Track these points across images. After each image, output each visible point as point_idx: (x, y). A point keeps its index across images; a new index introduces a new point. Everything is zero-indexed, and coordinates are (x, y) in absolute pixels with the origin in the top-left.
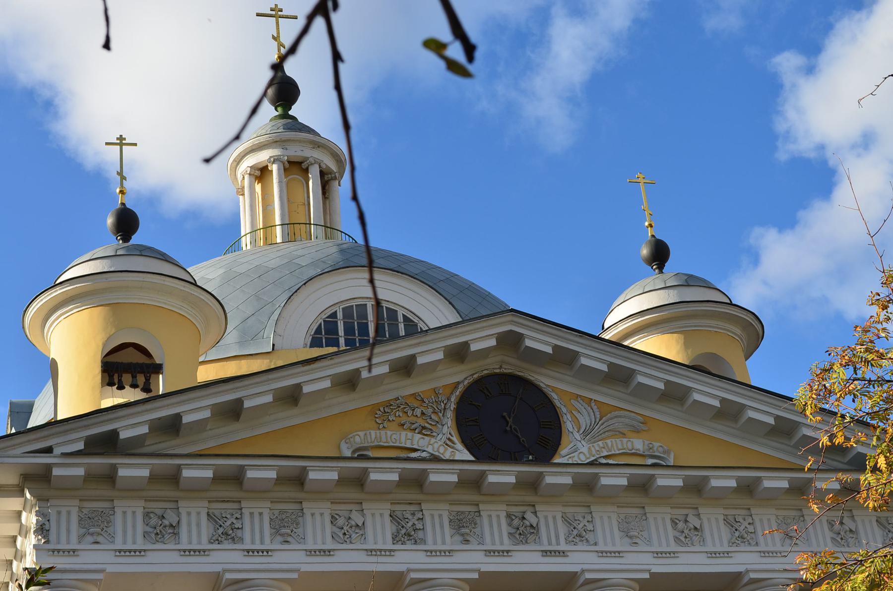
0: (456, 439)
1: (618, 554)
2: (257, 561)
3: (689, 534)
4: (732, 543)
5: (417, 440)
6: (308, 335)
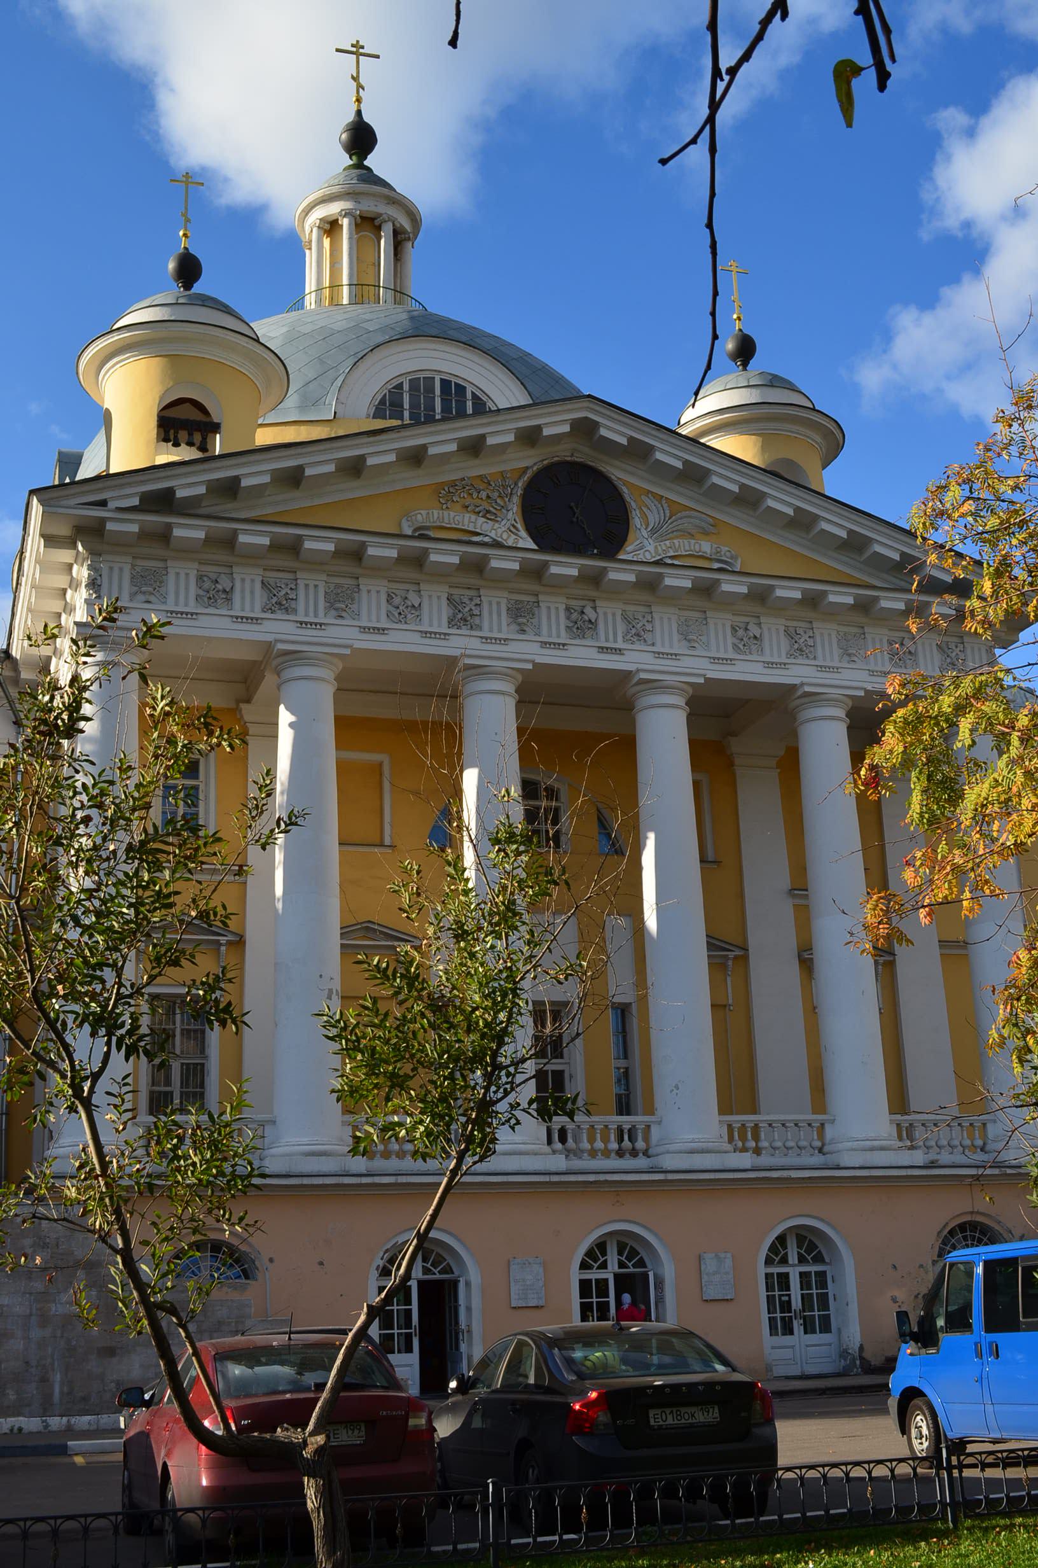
2: (310, 634)
5: (480, 524)
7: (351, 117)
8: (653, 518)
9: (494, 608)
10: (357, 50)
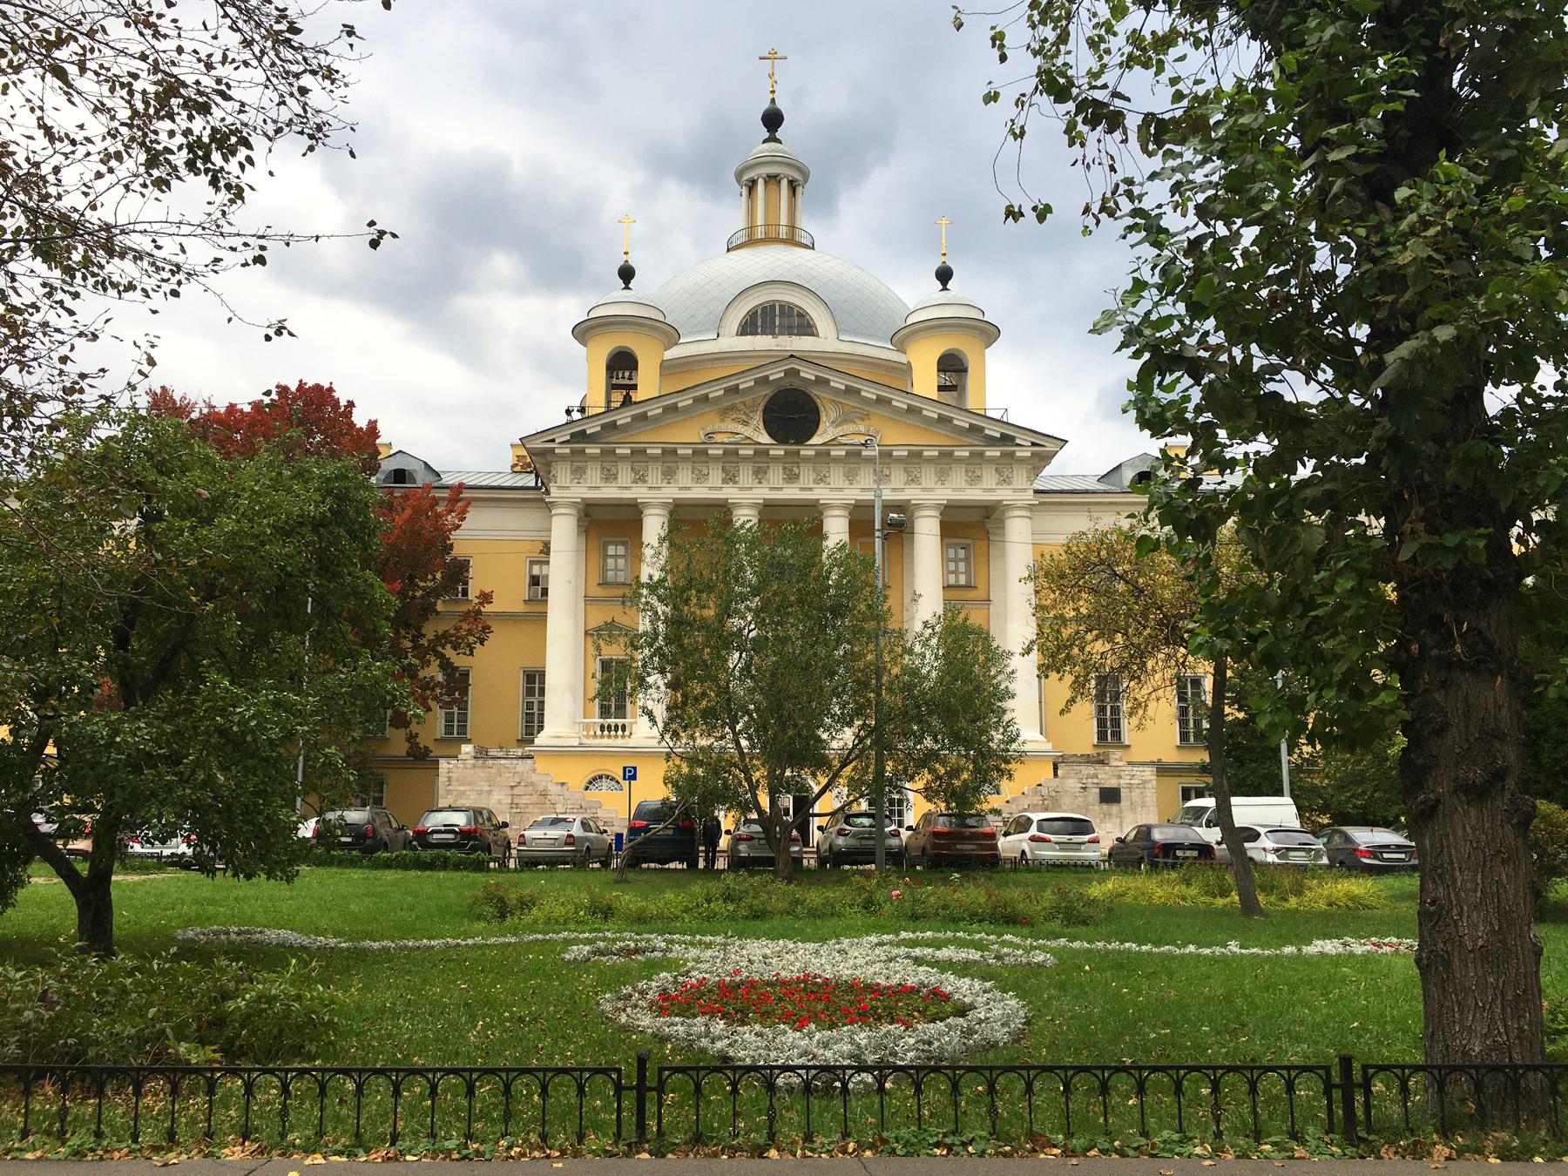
0: (761, 426)
1: (841, 489)
2: (653, 494)
3: (974, 479)
4: (815, 482)
5: (739, 428)
6: (591, 660)
7: (766, 105)
8: (833, 415)
9: (746, 475)
10: (772, 56)
